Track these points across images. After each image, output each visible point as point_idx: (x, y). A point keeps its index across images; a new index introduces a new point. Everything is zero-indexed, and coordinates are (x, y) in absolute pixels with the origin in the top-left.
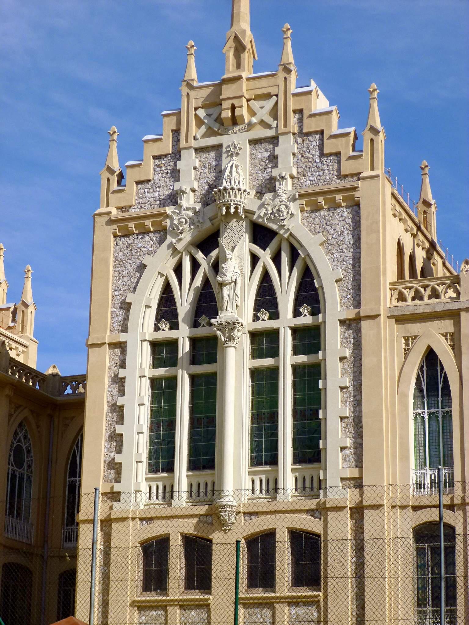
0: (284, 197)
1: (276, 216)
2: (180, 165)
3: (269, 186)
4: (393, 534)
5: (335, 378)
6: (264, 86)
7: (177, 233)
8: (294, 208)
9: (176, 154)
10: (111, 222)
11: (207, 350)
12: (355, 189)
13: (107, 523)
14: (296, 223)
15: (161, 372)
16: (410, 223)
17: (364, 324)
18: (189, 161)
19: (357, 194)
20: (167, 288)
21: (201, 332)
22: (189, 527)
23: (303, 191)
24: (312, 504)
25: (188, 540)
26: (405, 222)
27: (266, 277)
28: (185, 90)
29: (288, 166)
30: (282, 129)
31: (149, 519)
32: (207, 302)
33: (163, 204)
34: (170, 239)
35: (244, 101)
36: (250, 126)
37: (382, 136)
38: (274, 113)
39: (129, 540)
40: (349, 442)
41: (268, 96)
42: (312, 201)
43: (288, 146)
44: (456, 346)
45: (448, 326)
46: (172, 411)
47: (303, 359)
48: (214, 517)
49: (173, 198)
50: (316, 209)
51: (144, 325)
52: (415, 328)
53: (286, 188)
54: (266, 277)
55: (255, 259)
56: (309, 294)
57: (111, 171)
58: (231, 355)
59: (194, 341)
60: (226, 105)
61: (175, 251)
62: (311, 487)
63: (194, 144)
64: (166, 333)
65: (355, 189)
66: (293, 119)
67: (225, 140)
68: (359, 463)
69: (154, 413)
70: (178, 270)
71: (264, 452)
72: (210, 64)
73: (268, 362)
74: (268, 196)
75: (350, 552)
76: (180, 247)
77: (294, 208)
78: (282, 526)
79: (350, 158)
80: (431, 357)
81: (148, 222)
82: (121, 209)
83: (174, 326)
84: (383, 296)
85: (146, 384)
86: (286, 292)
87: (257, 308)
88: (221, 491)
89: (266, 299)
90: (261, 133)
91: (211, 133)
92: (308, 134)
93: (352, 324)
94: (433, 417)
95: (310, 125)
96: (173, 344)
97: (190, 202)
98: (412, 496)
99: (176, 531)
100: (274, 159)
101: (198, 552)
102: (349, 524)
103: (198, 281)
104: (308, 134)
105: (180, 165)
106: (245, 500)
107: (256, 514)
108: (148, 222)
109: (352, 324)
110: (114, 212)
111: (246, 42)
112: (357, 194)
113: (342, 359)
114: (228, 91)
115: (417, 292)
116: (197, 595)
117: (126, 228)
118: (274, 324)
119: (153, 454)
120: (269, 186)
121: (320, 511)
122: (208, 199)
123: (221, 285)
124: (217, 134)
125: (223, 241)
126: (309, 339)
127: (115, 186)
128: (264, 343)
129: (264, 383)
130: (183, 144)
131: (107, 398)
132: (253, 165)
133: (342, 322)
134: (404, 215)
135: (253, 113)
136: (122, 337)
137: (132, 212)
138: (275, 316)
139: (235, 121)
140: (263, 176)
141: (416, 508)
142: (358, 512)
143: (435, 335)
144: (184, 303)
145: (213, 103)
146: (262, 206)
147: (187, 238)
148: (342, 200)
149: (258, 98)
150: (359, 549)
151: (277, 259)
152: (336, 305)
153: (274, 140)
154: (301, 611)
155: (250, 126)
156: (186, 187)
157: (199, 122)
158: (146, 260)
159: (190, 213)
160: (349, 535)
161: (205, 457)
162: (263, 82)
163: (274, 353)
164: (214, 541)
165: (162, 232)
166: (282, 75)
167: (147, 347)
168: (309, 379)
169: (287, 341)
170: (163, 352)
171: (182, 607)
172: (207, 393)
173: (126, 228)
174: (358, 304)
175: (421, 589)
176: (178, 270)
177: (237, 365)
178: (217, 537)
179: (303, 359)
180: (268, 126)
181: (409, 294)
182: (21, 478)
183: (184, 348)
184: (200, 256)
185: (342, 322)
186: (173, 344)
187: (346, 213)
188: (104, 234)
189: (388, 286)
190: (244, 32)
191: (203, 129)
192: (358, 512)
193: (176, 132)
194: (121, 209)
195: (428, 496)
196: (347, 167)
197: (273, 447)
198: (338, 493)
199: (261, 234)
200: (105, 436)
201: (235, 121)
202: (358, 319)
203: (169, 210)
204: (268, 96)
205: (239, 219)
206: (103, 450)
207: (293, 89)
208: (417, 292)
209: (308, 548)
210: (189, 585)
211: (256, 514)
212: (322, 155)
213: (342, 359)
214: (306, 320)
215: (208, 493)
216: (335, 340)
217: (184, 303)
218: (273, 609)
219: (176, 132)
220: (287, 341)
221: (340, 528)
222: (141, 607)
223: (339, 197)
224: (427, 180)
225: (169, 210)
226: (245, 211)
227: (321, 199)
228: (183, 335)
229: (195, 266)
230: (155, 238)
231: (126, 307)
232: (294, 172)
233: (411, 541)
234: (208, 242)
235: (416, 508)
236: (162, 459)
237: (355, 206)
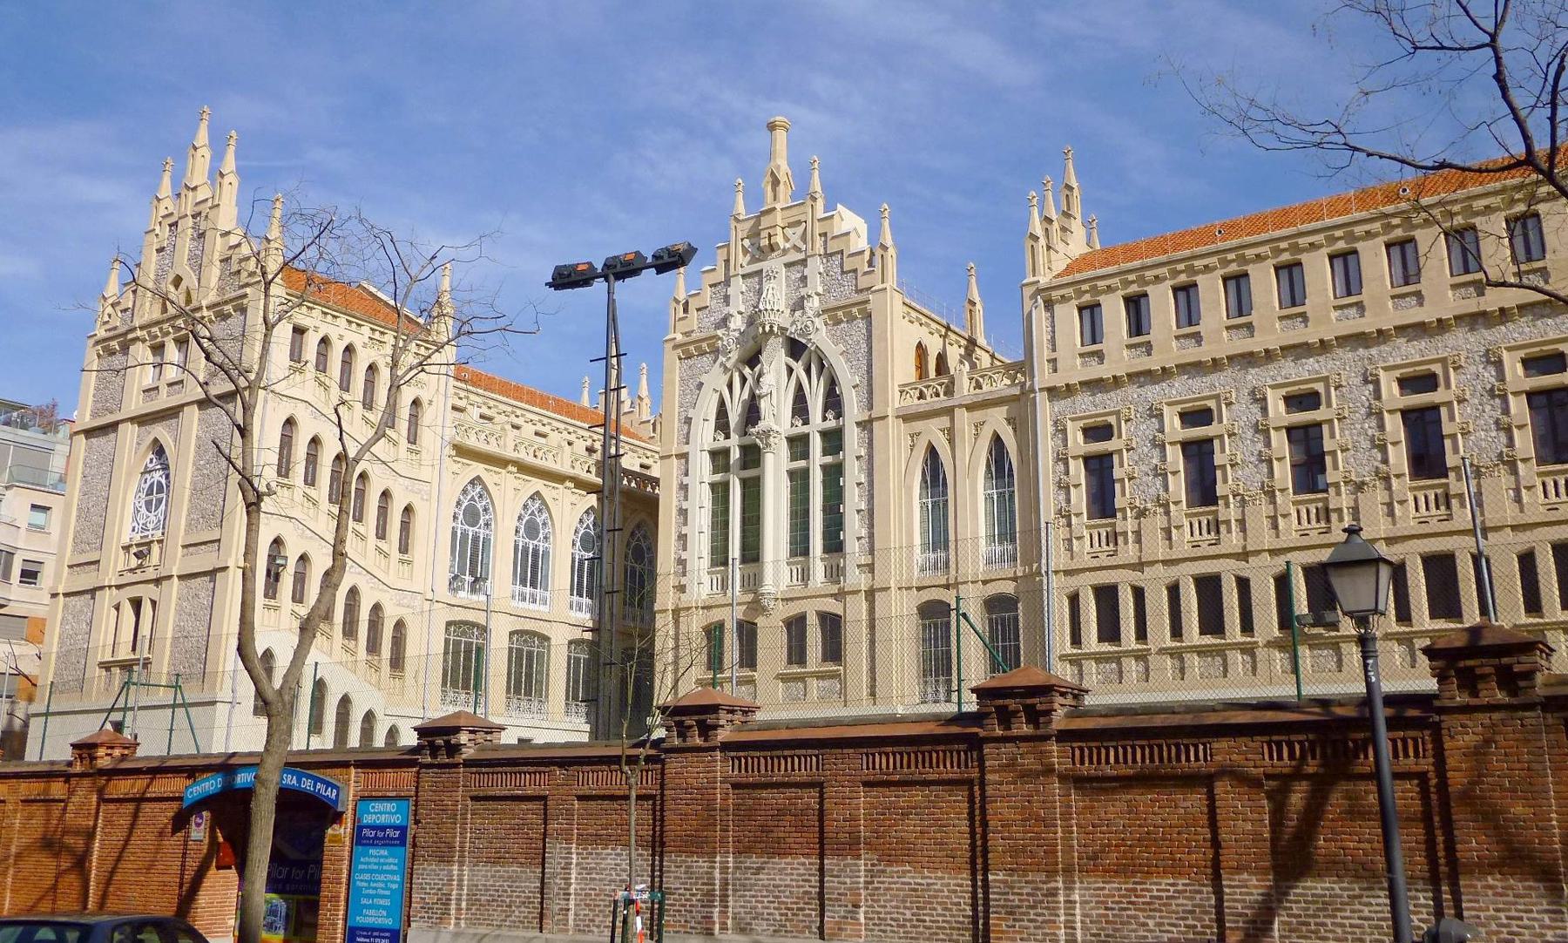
0: (810, 313)
1: (804, 332)
2: (730, 291)
3: (798, 305)
4: (900, 611)
5: (853, 474)
6: (795, 215)
7: (726, 353)
8: (819, 322)
9: (727, 283)
10: (676, 347)
11: (752, 456)
12: (867, 302)
13: (676, 612)
14: (821, 337)
15: (718, 477)
16: (934, 325)
17: (875, 424)
18: (738, 285)
19: (869, 307)
20: (722, 403)
21: (747, 441)
22: (739, 613)
23: (826, 307)
24: (834, 589)
25: (740, 624)
26: (928, 325)
27: (800, 388)
28: (733, 224)
29: (816, 285)
30: (810, 252)
31: (985, 582)
32: (752, 413)
33: (717, 327)
34: (722, 359)
35: (779, 230)
36: (785, 251)
37: (892, 251)
38: (804, 238)
39: (695, 624)
40: (864, 532)
41: (799, 223)
42: (834, 315)
43: (816, 266)
44: (951, 441)
45: (944, 421)
46: (726, 511)
47: (829, 459)
48: (757, 606)
49: (724, 322)
50: (838, 322)
51: (705, 436)
52: (918, 425)
53: (814, 304)
54: (800, 388)
55: (790, 370)
56: (833, 402)
57: (677, 302)
58: (769, 460)
59: (743, 448)
60: (764, 234)
61: (726, 369)
62: (835, 573)
63: (741, 271)
64: (722, 443)
65: (867, 302)
66: (819, 242)
67: (764, 265)
68: (872, 552)
69: (714, 514)
70: (730, 386)
71: (800, 546)
72: (753, 197)
73: (802, 463)
74: (798, 313)
75: (865, 631)
76: (729, 365)
77: (819, 322)
78: (811, 609)
79: (866, 273)
80: (932, 452)
81: (704, 345)
82: (686, 334)
83: (727, 437)
84: (893, 401)
85: (706, 489)
86: (816, 403)
87: (825, 410)
88: (761, 580)
89: (800, 408)
90: (794, 256)
91: (754, 260)
92: (831, 255)
93: (866, 425)
94: (1000, 495)
95: (833, 246)
96: (726, 452)
97: (737, 323)
98: (916, 577)
99: (730, 618)
100: (804, 279)
101: (748, 633)
102: (864, 605)
103: (746, 396)
104: (831, 255)
105: (730, 291)
106: (783, 587)
107: (792, 599)
108: (704, 345)
109: (866, 425)
110: (679, 337)
111: (782, 178)
112: (869, 307)
113: (858, 458)
114: (766, 222)
115: (921, 392)
116: (747, 672)
117: (688, 351)
118: (805, 429)
119: (714, 550)
120: (798, 305)
121: (840, 596)
122: (751, 321)
123: (760, 397)
124: (759, 260)
125: (763, 358)
126: (833, 441)
127: (681, 314)
128: (799, 445)
129: (799, 479)
130: (732, 272)
131: (675, 503)
132: (788, 286)
133: (858, 424)
134: (924, 320)
135: (787, 240)
136: (685, 449)
137: (694, 336)
138: (806, 422)
139: (772, 248)
140: (795, 296)
141: (919, 589)
142: (871, 594)
143: (933, 431)
144: (734, 417)
145: (754, 234)
146: (794, 323)
147: (734, 356)
148: (855, 313)
149: (790, 225)
150: (872, 626)
151: (808, 371)
152: (853, 408)
153: (803, 262)
154: (826, 683)
155: (785, 251)
156: (732, 310)
157: (745, 251)
158: (704, 378)
159: (737, 334)
160: (864, 616)
161: (752, 553)
162: (795, 211)
163: (805, 455)
164: (553, 642)
165: (716, 352)
166: (809, 203)
167: (706, 456)
168: (833, 474)
169: (816, 444)
170: (719, 458)
171: (1199, 654)
172: (752, 491)
173: (688, 351)
174: (871, 408)
175: (926, 659)
176: (730, 386)
177: (776, 468)
178: (760, 621)
179: (829, 459)
180: (798, 249)
181: (928, 393)
182: (641, 576)
183: (735, 454)
184: (747, 371)
185: (858, 424)
186: (726, 452)
187: (861, 324)
188: (671, 358)
189: (897, 389)
190: (778, 167)
191: (748, 257)
192: (871, 594)
193: (727, 261)
194: (686, 334)
195: (931, 578)
196: (863, 282)
197: (805, 539)
198: (856, 578)
199: (796, 348)
200: (674, 537)
201: (772, 248)
202: (871, 421)
203: (719, 333)
204: (799, 223)
205: (777, 336)
206: (673, 549)
207: (820, 214)
208: (921, 392)
209: (832, 625)
210: (1101, 639)
211: (792, 599)
212: (843, 272)
213: (858, 458)
214: (831, 424)
215: (753, 582)
216: (853, 440)
217: (734, 417)
218: (1119, 664)
219: (727, 261)
220: (816, 444)
221: (855, 611)
222: (785, 678)
223: (855, 310)
224: (973, 280)
225: (719, 333)
226: (780, 328)
227: (840, 313)
228: (734, 443)
229: (744, 380)
230: (710, 357)
231: (688, 421)
232: (820, 290)
233: (915, 619)
234: (753, 360)
235: (919, 589)
236: (720, 557)
237: (868, 317)
